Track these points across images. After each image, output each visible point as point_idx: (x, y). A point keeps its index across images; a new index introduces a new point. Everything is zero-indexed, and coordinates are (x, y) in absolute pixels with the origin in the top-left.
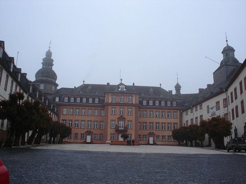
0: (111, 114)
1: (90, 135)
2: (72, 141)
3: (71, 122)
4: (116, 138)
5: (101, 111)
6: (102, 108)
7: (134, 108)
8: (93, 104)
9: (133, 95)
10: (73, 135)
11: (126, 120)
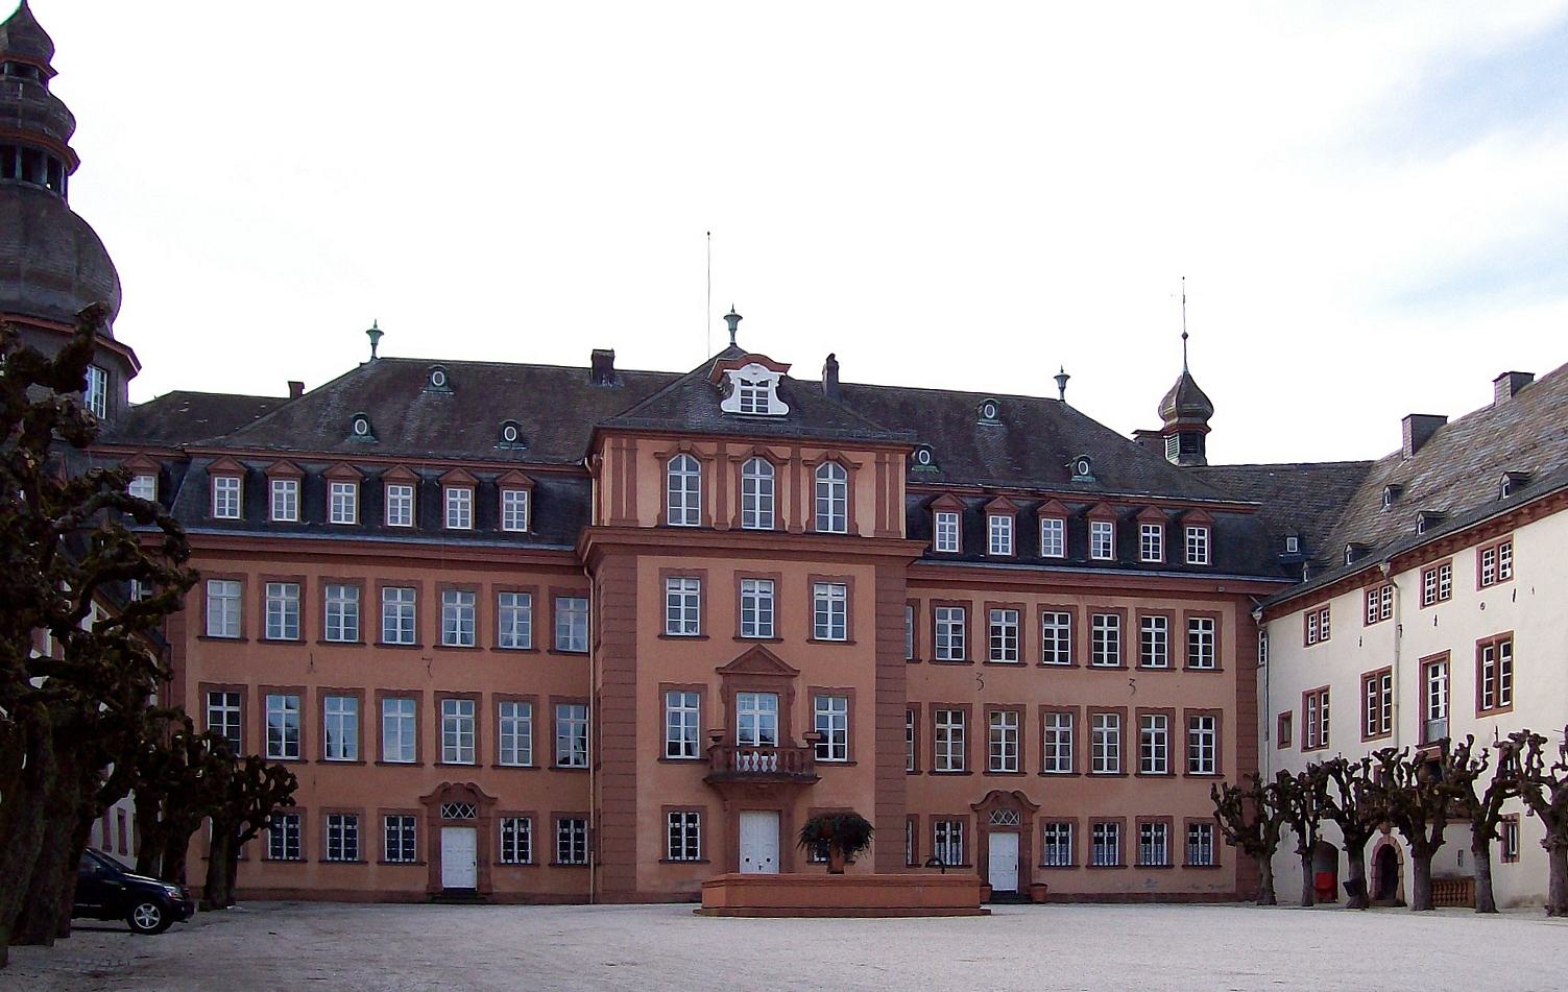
0: (663, 636)
1: (473, 825)
2: (310, 876)
3: (225, 709)
4: (715, 853)
5: (446, 605)
6: (571, 582)
7: (865, 576)
8: (484, 537)
9: (854, 457)
10: (315, 834)
11: (800, 687)
